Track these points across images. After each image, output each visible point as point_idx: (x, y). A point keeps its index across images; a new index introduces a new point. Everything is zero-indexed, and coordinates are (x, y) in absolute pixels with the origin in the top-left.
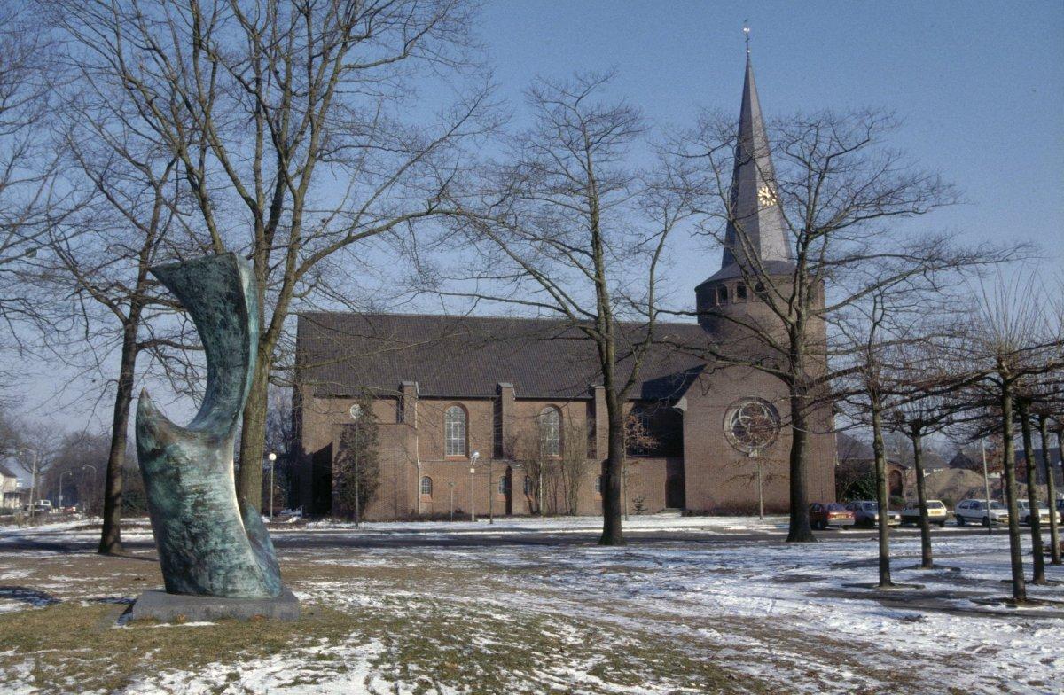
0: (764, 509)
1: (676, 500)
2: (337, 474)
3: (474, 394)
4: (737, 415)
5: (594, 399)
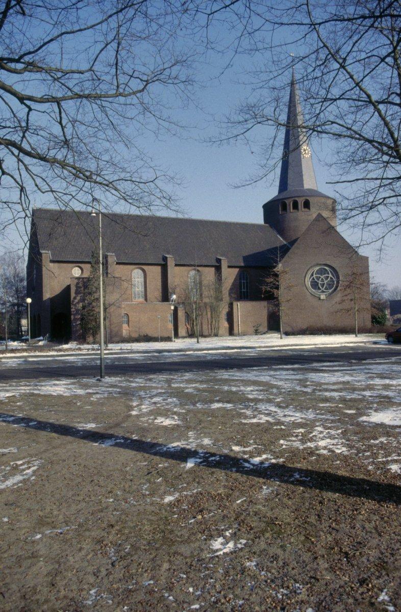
0: (10, 333)
1: (274, 324)
2: (74, 311)
3: (149, 262)
4: (312, 275)
5: (166, 264)
